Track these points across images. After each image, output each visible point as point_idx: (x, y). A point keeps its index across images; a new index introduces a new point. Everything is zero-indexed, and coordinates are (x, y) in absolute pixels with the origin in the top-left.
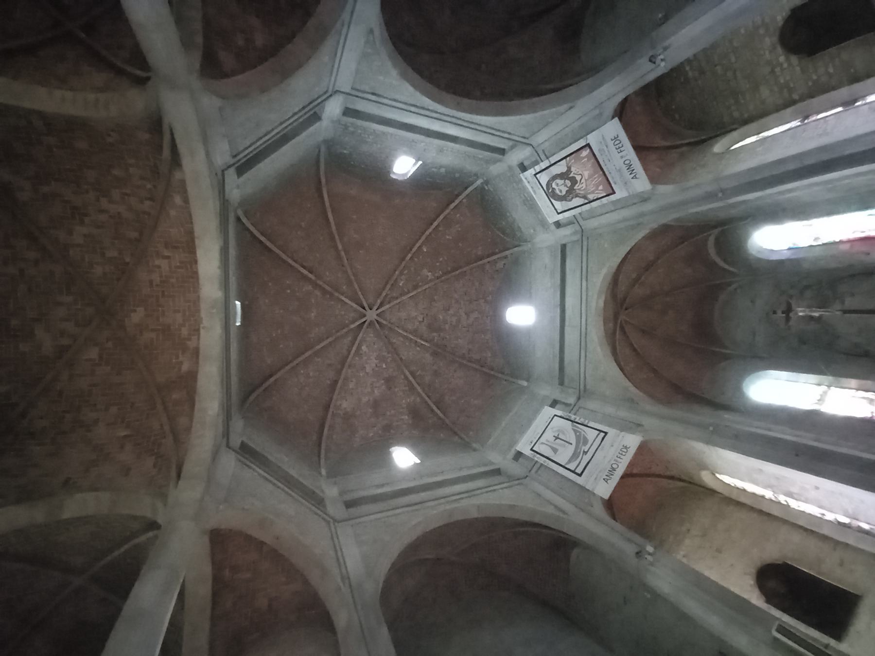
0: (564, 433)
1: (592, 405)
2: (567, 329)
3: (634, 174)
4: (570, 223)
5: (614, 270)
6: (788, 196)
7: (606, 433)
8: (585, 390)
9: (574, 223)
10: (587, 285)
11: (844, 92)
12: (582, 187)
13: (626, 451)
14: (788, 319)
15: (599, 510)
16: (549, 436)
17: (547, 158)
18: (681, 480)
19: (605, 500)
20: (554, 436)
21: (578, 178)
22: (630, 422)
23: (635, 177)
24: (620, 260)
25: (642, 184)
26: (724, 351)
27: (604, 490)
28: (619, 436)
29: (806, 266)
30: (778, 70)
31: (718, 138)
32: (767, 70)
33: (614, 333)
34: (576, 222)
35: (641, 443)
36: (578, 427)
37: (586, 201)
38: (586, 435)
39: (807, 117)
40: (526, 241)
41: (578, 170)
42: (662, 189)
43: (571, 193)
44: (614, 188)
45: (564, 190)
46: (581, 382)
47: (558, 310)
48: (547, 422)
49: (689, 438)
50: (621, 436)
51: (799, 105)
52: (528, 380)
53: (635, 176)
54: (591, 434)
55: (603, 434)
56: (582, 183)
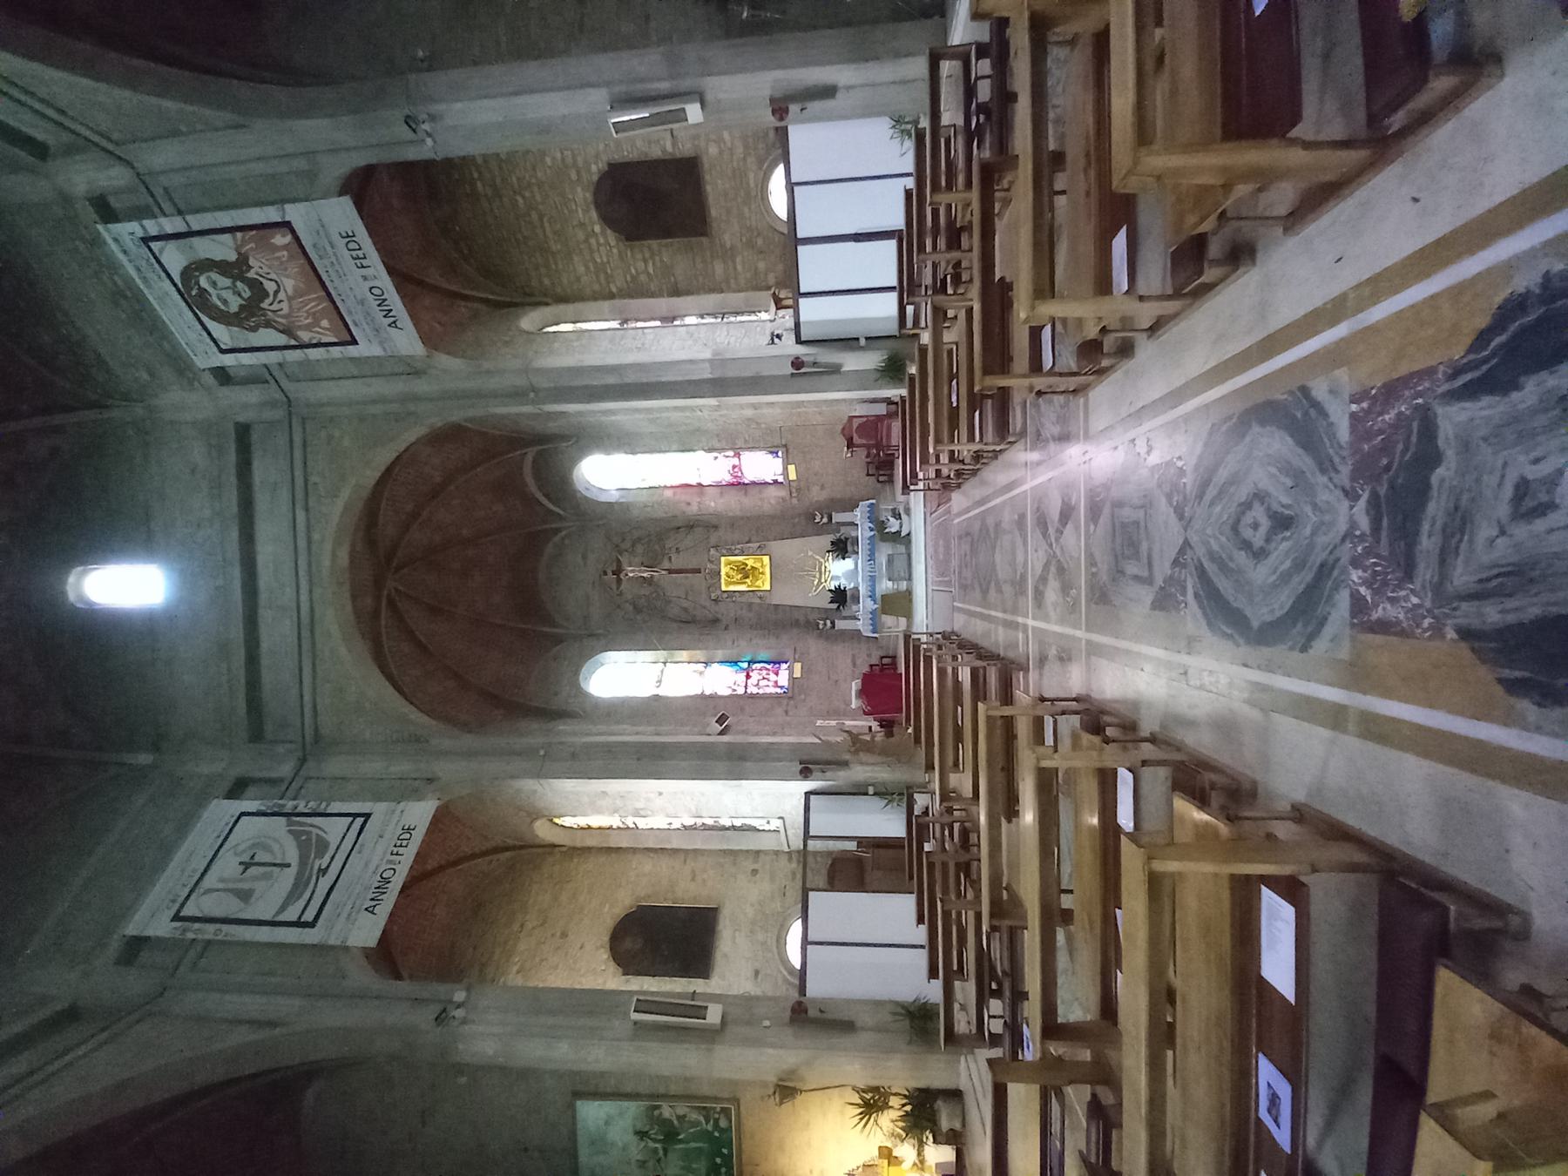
0: (267, 848)
1: (335, 766)
2: (265, 615)
3: (393, 319)
4: (254, 379)
5: (365, 493)
6: (618, 418)
7: (367, 816)
8: (317, 737)
9: (267, 382)
10: (308, 520)
11: (664, 304)
12: (281, 310)
13: (408, 836)
14: (619, 581)
15: (362, 976)
16: (228, 865)
17: (180, 213)
18: (507, 849)
19: (372, 949)
20: (241, 863)
21: (270, 287)
22: (415, 779)
23: (393, 324)
24: (377, 475)
25: (407, 341)
26: (556, 630)
27: (367, 932)
28: (394, 811)
29: (635, 513)
30: (593, 241)
31: (527, 308)
32: (581, 235)
33: (376, 614)
34: (269, 378)
35: (436, 811)
36: (301, 824)
37: (293, 342)
38: (324, 835)
39: (625, 321)
40: (126, 397)
41: (266, 270)
42: (444, 360)
43: (251, 313)
44: (354, 334)
45: (234, 304)
46: (307, 726)
47: (236, 572)
48: (219, 837)
49: (512, 777)
50: (398, 812)
51: (617, 302)
52: (156, 748)
53: (394, 322)
54: (333, 829)
55: (360, 820)
56: (280, 301)
